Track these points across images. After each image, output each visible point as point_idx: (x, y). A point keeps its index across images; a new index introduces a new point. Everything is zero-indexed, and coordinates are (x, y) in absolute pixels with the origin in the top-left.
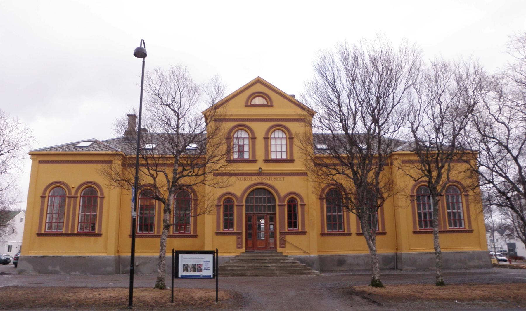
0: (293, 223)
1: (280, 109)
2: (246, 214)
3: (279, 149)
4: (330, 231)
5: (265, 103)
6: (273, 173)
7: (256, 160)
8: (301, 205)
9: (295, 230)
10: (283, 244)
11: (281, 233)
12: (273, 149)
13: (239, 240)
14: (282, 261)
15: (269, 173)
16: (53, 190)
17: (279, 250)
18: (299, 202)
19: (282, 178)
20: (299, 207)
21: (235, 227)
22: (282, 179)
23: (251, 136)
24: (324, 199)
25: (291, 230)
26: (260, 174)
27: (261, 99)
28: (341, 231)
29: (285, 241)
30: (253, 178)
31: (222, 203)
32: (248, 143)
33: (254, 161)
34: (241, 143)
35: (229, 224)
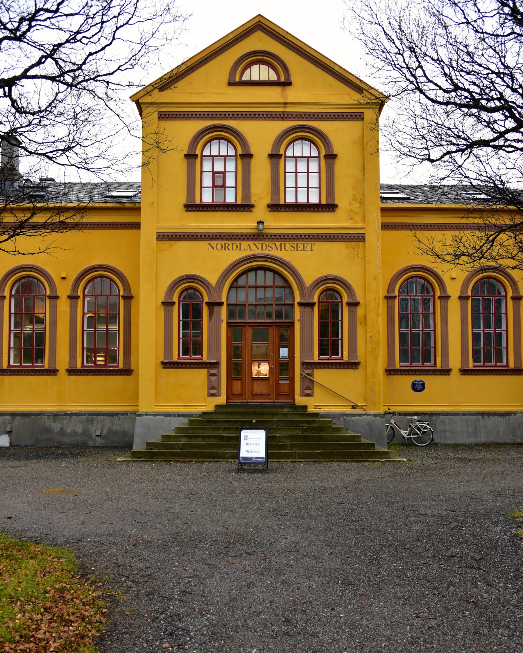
0: (329, 342)
1: (308, 91)
2: (201, 327)
3: (302, 183)
4: (406, 365)
5: (274, 77)
6: (288, 235)
7: (253, 206)
8: (348, 304)
9: (335, 359)
10: (309, 387)
11: (306, 365)
12: (290, 182)
13: (213, 378)
14: (305, 426)
15: (280, 235)
16: (325, 293)
17: (299, 400)
18: (345, 299)
19: (308, 245)
20: (346, 309)
21: (205, 352)
22: (309, 247)
23: (240, 152)
24: (467, 298)
25: (325, 358)
26: (259, 235)
27: (264, 68)
28: (428, 365)
29: (312, 382)
30: (245, 244)
31: (175, 299)
32: (234, 170)
33: (246, 207)
34: (219, 167)
35: (192, 346)
